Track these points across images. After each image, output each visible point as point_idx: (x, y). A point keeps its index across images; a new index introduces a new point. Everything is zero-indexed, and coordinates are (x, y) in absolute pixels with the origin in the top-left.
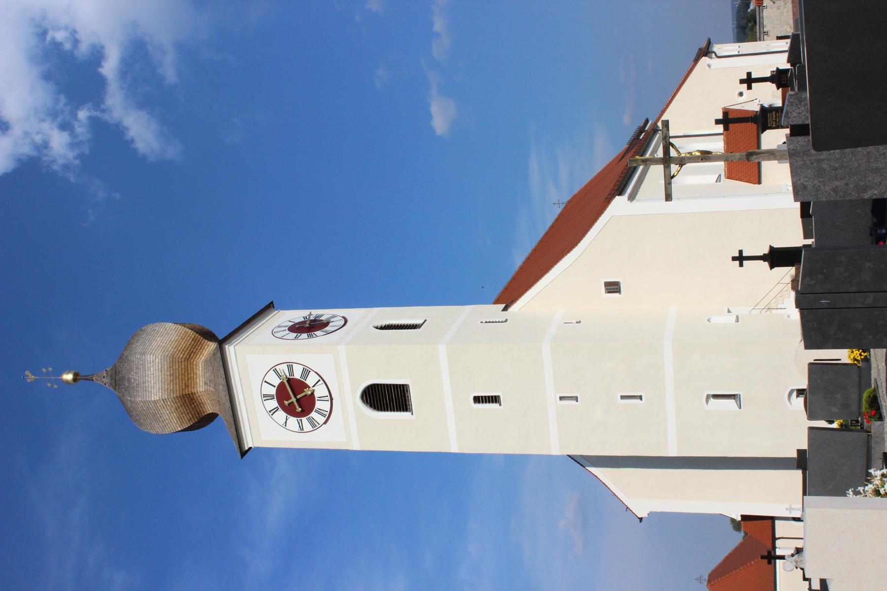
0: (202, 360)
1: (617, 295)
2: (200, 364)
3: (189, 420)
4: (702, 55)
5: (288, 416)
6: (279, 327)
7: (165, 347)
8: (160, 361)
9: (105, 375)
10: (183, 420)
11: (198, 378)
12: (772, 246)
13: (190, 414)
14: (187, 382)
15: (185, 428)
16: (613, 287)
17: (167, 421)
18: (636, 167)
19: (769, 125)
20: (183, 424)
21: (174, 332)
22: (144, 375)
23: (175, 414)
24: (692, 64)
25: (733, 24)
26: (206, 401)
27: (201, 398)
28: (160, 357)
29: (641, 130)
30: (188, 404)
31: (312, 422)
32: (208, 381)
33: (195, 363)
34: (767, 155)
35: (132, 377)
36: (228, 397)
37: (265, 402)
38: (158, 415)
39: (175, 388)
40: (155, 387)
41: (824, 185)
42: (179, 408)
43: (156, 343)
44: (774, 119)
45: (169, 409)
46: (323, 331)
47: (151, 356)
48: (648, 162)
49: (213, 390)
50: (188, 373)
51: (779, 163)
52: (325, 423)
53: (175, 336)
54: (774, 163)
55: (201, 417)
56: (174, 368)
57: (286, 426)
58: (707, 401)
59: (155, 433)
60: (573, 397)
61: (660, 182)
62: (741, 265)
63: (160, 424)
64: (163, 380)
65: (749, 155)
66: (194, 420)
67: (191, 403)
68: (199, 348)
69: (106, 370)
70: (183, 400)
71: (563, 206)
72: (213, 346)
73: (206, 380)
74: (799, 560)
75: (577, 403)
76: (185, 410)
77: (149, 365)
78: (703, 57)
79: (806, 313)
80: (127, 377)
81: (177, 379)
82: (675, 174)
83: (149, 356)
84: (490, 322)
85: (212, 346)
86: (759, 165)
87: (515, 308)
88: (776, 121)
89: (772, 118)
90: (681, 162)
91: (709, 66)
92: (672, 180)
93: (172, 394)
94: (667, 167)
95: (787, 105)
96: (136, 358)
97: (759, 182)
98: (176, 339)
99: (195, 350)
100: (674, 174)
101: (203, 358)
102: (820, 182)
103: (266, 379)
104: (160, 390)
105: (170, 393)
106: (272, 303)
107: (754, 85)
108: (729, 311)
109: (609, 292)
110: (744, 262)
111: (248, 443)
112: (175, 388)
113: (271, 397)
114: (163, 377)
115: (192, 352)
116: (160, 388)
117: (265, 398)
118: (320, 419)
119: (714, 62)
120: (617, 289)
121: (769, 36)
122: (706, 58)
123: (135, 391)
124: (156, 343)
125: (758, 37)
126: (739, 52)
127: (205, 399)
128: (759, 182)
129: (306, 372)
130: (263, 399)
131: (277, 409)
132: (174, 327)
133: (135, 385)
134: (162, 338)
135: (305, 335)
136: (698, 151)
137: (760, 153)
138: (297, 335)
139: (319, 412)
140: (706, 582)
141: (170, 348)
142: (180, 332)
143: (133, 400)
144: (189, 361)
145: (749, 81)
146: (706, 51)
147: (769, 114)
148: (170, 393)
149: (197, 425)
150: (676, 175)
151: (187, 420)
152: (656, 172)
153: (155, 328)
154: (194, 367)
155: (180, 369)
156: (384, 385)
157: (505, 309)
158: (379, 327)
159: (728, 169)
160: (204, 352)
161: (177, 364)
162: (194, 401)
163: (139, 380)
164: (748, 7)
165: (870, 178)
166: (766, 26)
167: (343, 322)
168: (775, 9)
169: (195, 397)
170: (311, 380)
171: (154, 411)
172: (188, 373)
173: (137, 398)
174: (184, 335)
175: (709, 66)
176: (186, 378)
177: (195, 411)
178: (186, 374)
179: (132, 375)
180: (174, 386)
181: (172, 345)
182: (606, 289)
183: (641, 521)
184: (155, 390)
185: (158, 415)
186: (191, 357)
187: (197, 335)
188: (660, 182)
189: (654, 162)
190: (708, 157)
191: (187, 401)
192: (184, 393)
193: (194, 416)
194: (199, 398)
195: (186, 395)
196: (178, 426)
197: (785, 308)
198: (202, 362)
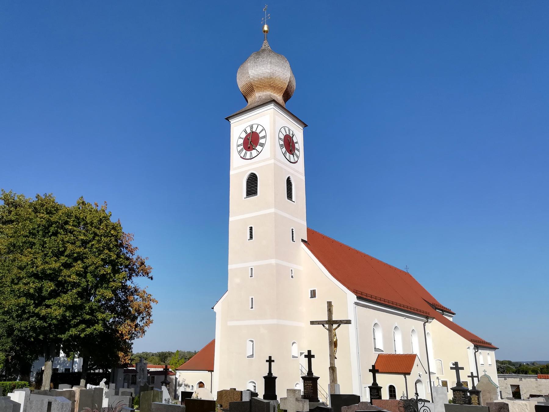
5: (243, 139)
8: (267, 72)
14: (259, 87)
16: (313, 294)
27: (253, 95)
31: (242, 150)
33: (269, 90)
34: (333, 378)
37: (249, 127)
52: (241, 157)
62: (267, 361)
68: (278, 91)
71: (405, 271)
81: (260, 82)
84: (293, 233)
90: (330, 330)
91: (469, 348)
93: (252, 80)
94: (327, 322)
99: (276, 89)
100: (325, 326)
117: (251, 127)
119: (472, 350)
120: (312, 296)
121: (519, 381)
136: (337, 340)
139: (246, 154)
142: (285, 80)
154: (267, 90)
155: (265, 83)
157: (303, 241)
159: (386, 356)
166: (525, 379)
168: (536, 385)
170: (259, 148)
175: (469, 348)
176: (261, 87)
181: (277, 77)
183: (212, 308)
184: (253, 72)
187: (285, 89)
190: (332, 344)
191: (251, 88)
192: (254, 86)
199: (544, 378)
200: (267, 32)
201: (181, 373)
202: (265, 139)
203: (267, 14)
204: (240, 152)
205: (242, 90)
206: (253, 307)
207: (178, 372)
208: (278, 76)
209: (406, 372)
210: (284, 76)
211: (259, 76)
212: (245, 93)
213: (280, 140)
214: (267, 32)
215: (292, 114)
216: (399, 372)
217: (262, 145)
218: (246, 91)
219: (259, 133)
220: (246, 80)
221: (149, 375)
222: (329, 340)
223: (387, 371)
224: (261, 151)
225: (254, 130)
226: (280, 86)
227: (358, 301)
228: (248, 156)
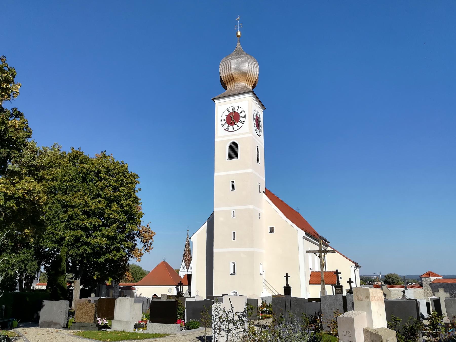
1: (269, 231)
5: (227, 116)
6: (258, 112)
14: (238, 79)
16: (272, 230)
18: (318, 241)
29: (326, 240)
30: (230, 79)
31: (225, 124)
36: (233, 94)
37: (231, 108)
39: (236, 74)
41: (326, 306)
51: (320, 291)
52: (224, 129)
56: (243, 74)
58: (233, 263)
60: (234, 215)
62: (285, 277)
79: (284, 298)
85: (251, 88)
86: (320, 284)
87: (264, 195)
88: (338, 291)
91: (351, 267)
93: (234, 73)
94: (318, 252)
97: (310, 284)
102: (327, 305)
106: (266, 109)
107: (349, 283)
108: (264, 271)
109: (270, 229)
110: (286, 278)
111: (217, 101)
112: (236, 74)
117: (233, 108)
118: (225, 127)
119: (353, 269)
120: (271, 231)
128: (310, 284)
129: (242, 122)
131: (229, 112)
135: (255, 122)
136: (325, 262)
137: (324, 285)
139: (228, 127)
145: (350, 282)
146: (357, 266)
149: (223, 82)
152: (317, 248)
154: (243, 81)
155: (243, 76)
159: (316, 273)
161: (245, 75)
167: (259, 135)
170: (239, 124)
175: (351, 267)
176: (239, 79)
182: (271, 228)
191: (231, 79)
192: (234, 78)
195: (233, 78)
200: (239, 37)
201: (138, 288)
202: (244, 118)
203: (240, 24)
204: (223, 125)
205: (224, 79)
206: (235, 239)
207: (136, 287)
209: (333, 283)
212: (226, 82)
215: (260, 101)
216: (328, 283)
217: (242, 122)
218: (226, 80)
220: (229, 72)
221: (120, 290)
223: (314, 283)
224: (241, 127)
225: (236, 111)
226: (252, 80)
227: (305, 236)
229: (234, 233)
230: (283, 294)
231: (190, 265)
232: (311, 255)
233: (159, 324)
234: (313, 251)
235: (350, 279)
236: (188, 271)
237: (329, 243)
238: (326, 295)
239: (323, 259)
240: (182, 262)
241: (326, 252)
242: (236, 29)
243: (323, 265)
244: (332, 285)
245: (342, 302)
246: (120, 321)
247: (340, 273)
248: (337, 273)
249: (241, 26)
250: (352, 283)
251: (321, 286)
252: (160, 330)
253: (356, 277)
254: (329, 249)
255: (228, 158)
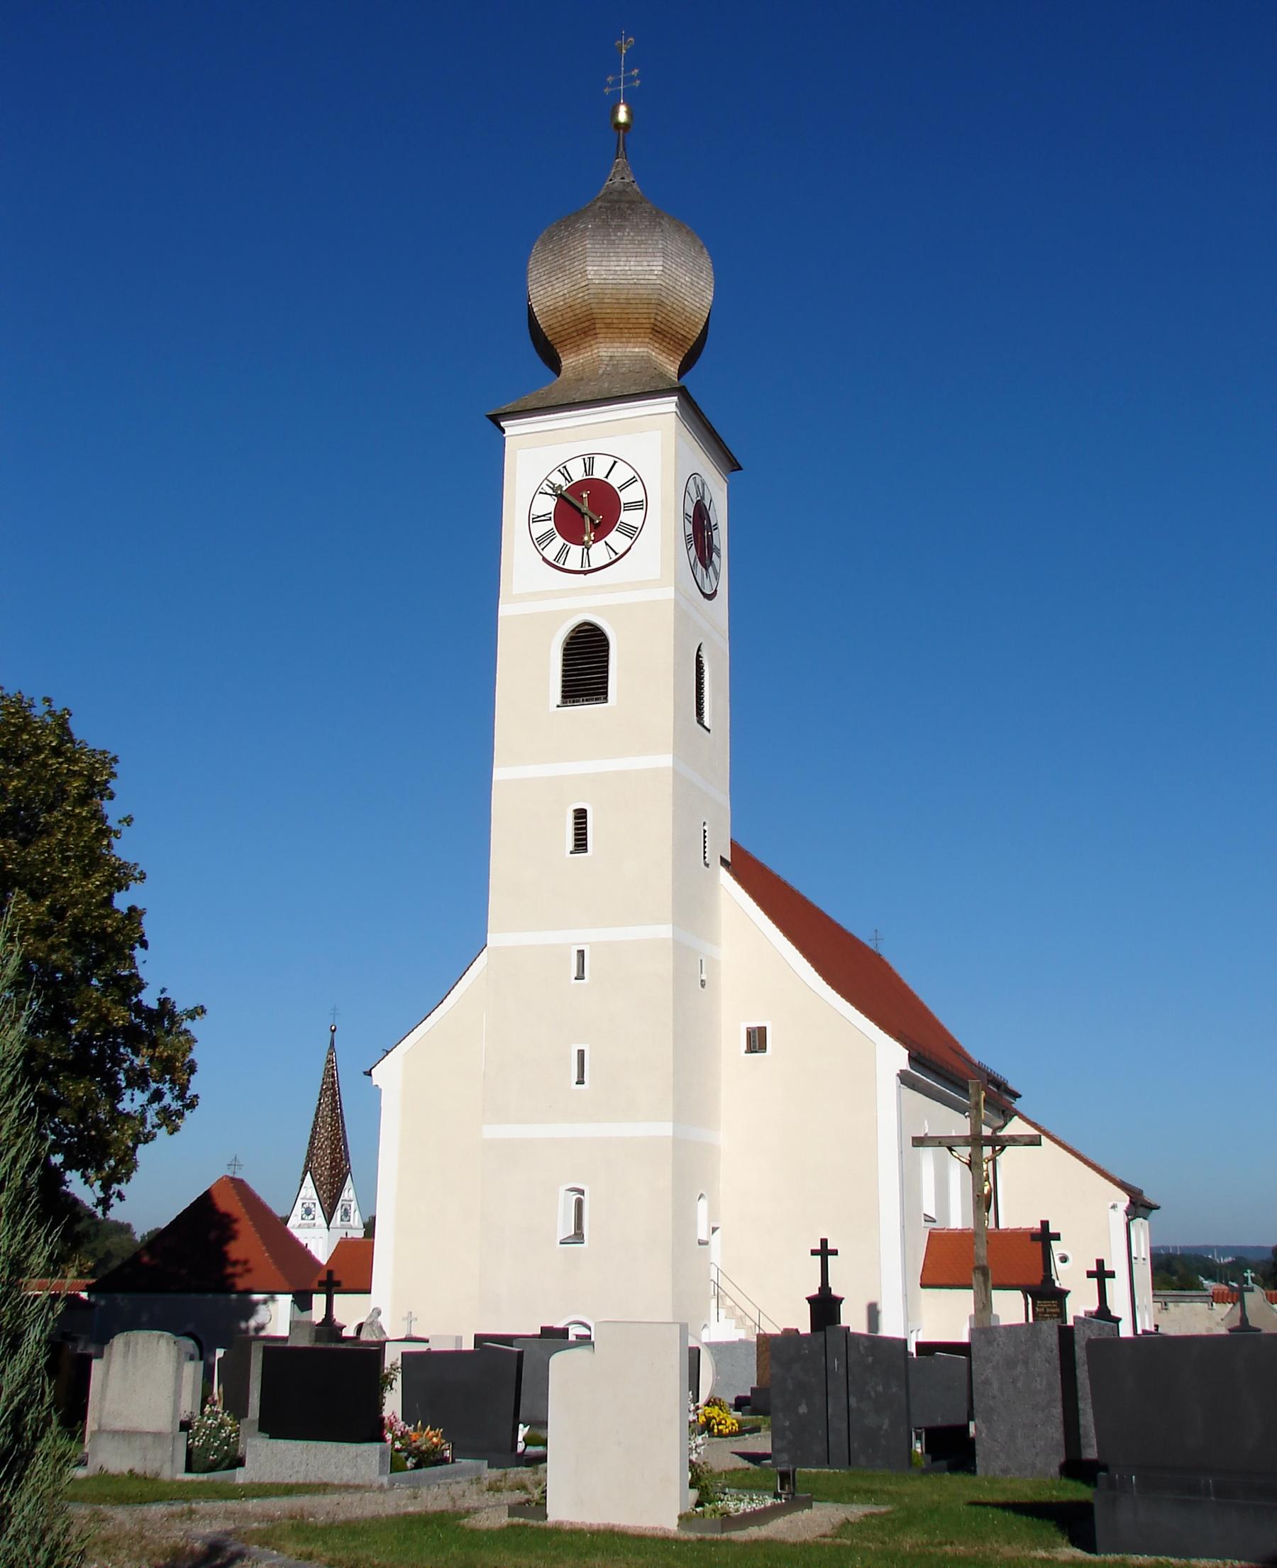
0: (650, 351)
1: (744, 1046)
2: (646, 350)
3: (549, 326)
4: (1132, 1196)
6: (703, 485)
7: (674, 290)
8: (651, 282)
9: (627, 180)
10: (551, 317)
11: (621, 345)
12: (843, 1302)
13: (560, 328)
14: (615, 326)
15: (538, 318)
16: (756, 1040)
17: (550, 288)
19: (1038, 1302)
20: (545, 315)
21: (698, 305)
22: (629, 254)
23: (562, 303)
24: (1119, 1176)
25: (1175, 1248)
26: (581, 356)
27: (588, 349)
28: (658, 282)
31: (545, 539)
32: (615, 362)
35: (626, 234)
36: (590, 398)
37: (580, 460)
38: (560, 275)
39: (606, 305)
40: (609, 272)
42: (572, 311)
43: (681, 275)
44: (1048, 1310)
45: (571, 294)
46: (695, 558)
47: (661, 268)
48: (975, 1111)
49: (601, 372)
50: (631, 328)
51: (970, 1317)
52: (544, 559)
53: (692, 306)
54: (971, 1310)
55: (555, 346)
56: (640, 306)
57: (540, 493)
59: (531, 267)
61: (953, 1131)
62: (814, 1253)
63: (545, 277)
64: (620, 286)
65: (984, 1271)
66: (549, 336)
67: (580, 332)
68: (670, 347)
69: (633, 182)
70: (584, 319)
71: (871, 945)
72: (672, 369)
73: (617, 358)
74: (374, 1328)
75: (574, 978)
76: (568, 320)
77: (645, 263)
78: (1128, 1198)
80: (627, 223)
82: (953, 1152)
83: (661, 263)
85: (672, 369)
86: (969, 1287)
88: (1045, 1312)
89: (1049, 1307)
90: (973, 1164)
91: (1114, 1207)
92: (946, 1148)
93: (596, 300)
94: (967, 1141)
95: (1100, 1323)
96: (657, 241)
98: (687, 309)
101: (653, 354)
103: (619, 463)
104: (603, 281)
105: (598, 298)
106: (740, 468)
110: (1095, 1279)
111: (512, 428)
112: (606, 305)
113: (589, 468)
114: (626, 287)
115: (664, 335)
116: (607, 281)
118: (551, 552)
119: (1119, 1217)
120: (754, 1047)
122: (1128, 1202)
123: (602, 238)
124: (681, 275)
125: (1158, 1292)
126: (1135, 1258)
127: (586, 355)
128: (923, 1286)
130: (586, 457)
132: (706, 305)
133: (613, 238)
134: (688, 284)
135: (690, 530)
138: (690, 517)
139: (563, 551)
140: (231, 1175)
141: (672, 300)
143: (588, 234)
144: (650, 330)
146: (1139, 1207)
147: (1056, 1302)
148: (598, 298)
150: (952, 1154)
151: (550, 323)
152: (959, 1125)
153: (705, 272)
154: (640, 339)
155: (637, 316)
156: (607, 661)
158: (700, 653)
160: (664, 354)
162: (583, 335)
163: (621, 246)
164: (1210, 1277)
165: (1002, 1427)
166: (1178, 1306)
167: (708, 592)
169: (589, 338)
170: (616, 539)
171: (567, 268)
172: (631, 328)
173: (591, 241)
174: (693, 323)
175: (1114, 1207)
176: (622, 326)
177: (566, 337)
178: (628, 326)
179: (629, 233)
180: (610, 306)
181: (676, 302)
183: (365, 1073)
185: (560, 275)
186: (657, 334)
188: (953, 1131)
189: (976, 1122)
190: (982, 1205)
191: (584, 325)
192: (597, 321)
193: (557, 335)
194: (587, 344)
196: (541, 307)
197: (718, 1320)
198: (648, 352)
199: (1232, 1299)
208: (680, 299)
210: (697, 300)
211: (621, 291)
213: (686, 520)
214: (626, 126)
217: (632, 532)
219: (622, 488)
222: (973, 1190)
228: (574, 561)
229: (583, 1051)
230: (805, 1328)
231: (342, 1198)
232: (928, 1156)
233: (301, 1444)
234: (943, 1140)
235: (1100, 1263)
236: (328, 1224)
237: (1016, 1095)
238: (993, 1324)
239: (988, 1175)
240: (303, 1180)
241: (999, 1144)
242: (612, 92)
243: (985, 1201)
244: (1026, 1290)
245: (1056, 1352)
246: (128, 1435)
247: (1057, 1237)
248: (1044, 1236)
249: (633, 79)
250: (1107, 1280)
251: (974, 1292)
252: (303, 1468)
253: (1134, 1255)
254: (1016, 1127)
255: (558, 700)
